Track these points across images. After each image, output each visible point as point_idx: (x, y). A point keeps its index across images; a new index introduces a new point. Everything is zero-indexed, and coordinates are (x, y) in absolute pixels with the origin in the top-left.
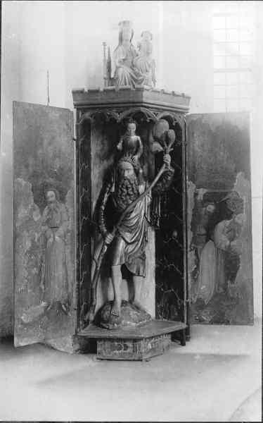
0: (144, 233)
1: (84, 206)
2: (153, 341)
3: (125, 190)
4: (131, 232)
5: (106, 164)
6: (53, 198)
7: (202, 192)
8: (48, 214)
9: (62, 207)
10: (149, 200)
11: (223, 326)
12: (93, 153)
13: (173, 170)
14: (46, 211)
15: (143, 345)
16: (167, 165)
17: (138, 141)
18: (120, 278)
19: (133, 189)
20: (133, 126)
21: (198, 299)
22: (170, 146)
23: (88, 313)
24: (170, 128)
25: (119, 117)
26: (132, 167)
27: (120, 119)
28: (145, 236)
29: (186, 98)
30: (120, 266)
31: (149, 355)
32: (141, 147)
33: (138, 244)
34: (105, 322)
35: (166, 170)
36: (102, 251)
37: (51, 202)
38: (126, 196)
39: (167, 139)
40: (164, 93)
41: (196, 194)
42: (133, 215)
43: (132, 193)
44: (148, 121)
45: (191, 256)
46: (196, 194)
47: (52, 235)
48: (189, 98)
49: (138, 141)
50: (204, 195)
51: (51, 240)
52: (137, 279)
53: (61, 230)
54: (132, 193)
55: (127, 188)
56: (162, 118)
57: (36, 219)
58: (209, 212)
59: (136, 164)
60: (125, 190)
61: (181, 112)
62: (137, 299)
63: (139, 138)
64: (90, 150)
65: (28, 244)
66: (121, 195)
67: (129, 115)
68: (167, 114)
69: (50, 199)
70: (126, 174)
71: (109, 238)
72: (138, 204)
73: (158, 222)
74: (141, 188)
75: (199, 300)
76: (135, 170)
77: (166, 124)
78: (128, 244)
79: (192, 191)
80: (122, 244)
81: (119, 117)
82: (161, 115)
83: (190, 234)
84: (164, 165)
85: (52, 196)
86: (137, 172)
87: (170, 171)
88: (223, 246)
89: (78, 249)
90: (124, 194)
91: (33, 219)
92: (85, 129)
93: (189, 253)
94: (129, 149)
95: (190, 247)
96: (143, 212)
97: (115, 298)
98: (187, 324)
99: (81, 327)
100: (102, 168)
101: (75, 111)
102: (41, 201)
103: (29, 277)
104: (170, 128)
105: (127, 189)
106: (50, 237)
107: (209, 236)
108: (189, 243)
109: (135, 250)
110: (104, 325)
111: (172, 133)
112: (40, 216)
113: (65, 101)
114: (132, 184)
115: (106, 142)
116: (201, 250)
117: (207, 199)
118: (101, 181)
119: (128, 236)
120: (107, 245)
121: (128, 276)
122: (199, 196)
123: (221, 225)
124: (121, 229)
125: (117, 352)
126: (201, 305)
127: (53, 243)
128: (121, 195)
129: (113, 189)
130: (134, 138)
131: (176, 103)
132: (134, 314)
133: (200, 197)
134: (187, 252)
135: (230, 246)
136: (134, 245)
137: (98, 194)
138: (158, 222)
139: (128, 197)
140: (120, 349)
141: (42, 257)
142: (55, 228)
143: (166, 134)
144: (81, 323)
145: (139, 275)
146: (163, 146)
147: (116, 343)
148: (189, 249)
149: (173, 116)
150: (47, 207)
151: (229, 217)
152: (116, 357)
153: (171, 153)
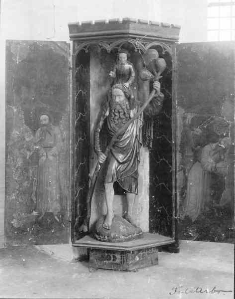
0: (136, 154)
1: (82, 125)
2: (141, 253)
3: (117, 114)
4: (122, 153)
5: (104, 89)
6: (47, 122)
7: (190, 116)
8: (41, 135)
9: (56, 130)
10: (140, 123)
11: (173, 254)
12: (92, 82)
13: (162, 95)
14: (38, 133)
15: (130, 258)
16: (156, 91)
17: (130, 69)
18: (113, 192)
19: (125, 113)
20: (124, 56)
21: (186, 216)
22: (159, 74)
23: (83, 226)
24: (160, 57)
25: (109, 48)
26: (122, 94)
27: (110, 50)
28: (137, 156)
29: (176, 29)
30: (112, 184)
31: (137, 267)
32: (133, 74)
33: (129, 165)
34: (98, 234)
35: (156, 95)
36: (96, 169)
37: (44, 125)
38: (118, 120)
39: (157, 67)
40: (152, 24)
41: (184, 118)
42: (126, 136)
43: (123, 117)
44: (164, 53)
45: (179, 176)
46: (184, 118)
47: (45, 154)
48: (179, 28)
49: (130, 69)
50: (193, 119)
51: (44, 158)
52: (131, 196)
53: (54, 150)
54: (123, 117)
55: (119, 112)
56: (151, 48)
57: (27, 139)
58: (197, 135)
59: (127, 91)
60: (117, 114)
61: (171, 42)
62: (130, 213)
63: (131, 66)
64: (88, 77)
65: (20, 163)
66: (113, 119)
67: (118, 46)
68: (156, 44)
69: (44, 122)
70: (117, 100)
71: (102, 158)
72: (129, 128)
73: (151, 143)
74: (132, 113)
75: (187, 217)
76: (126, 96)
77: (155, 53)
78: (120, 163)
79: (180, 116)
80: (114, 166)
81: (109, 48)
82: (150, 45)
83: (179, 156)
84: (154, 91)
85: (45, 120)
86: (128, 98)
87: (159, 97)
88: (209, 167)
89: (73, 167)
90: (116, 118)
91: (25, 139)
92: (83, 59)
93: (178, 173)
94: (122, 76)
95: (179, 168)
96: (135, 133)
97: (108, 213)
98: (176, 239)
99: (75, 238)
100: (100, 94)
101: (71, 43)
102: (34, 125)
103: (21, 189)
104: (160, 57)
105: (120, 117)
106: (43, 155)
107: (197, 159)
108: (178, 164)
109: (129, 168)
110: (97, 236)
111: (162, 62)
112: (32, 137)
113: (63, 36)
114: (123, 109)
115: (102, 70)
116: (189, 170)
117: (196, 122)
118: (99, 106)
119: (121, 157)
120: (100, 164)
121: (119, 190)
122: (187, 120)
123: (207, 148)
124: (114, 150)
125: (107, 262)
126: (188, 220)
127: (45, 161)
128: (113, 119)
129: (107, 113)
130: (128, 66)
131: (169, 35)
132: (124, 228)
133: (188, 121)
134: (176, 172)
135: (215, 167)
136: (126, 164)
137: (96, 117)
138: (151, 143)
139: (120, 121)
140: (110, 259)
141: (33, 172)
142: (48, 148)
143: (155, 61)
144: (75, 233)
145: (131, 192)
146: (153, 73)
147: (106, 254)
148: (178, 169)
149: (162, 46)
150: (39, 129)
151: (214, 142)
152: (105, 267)
153: (160, 80)
